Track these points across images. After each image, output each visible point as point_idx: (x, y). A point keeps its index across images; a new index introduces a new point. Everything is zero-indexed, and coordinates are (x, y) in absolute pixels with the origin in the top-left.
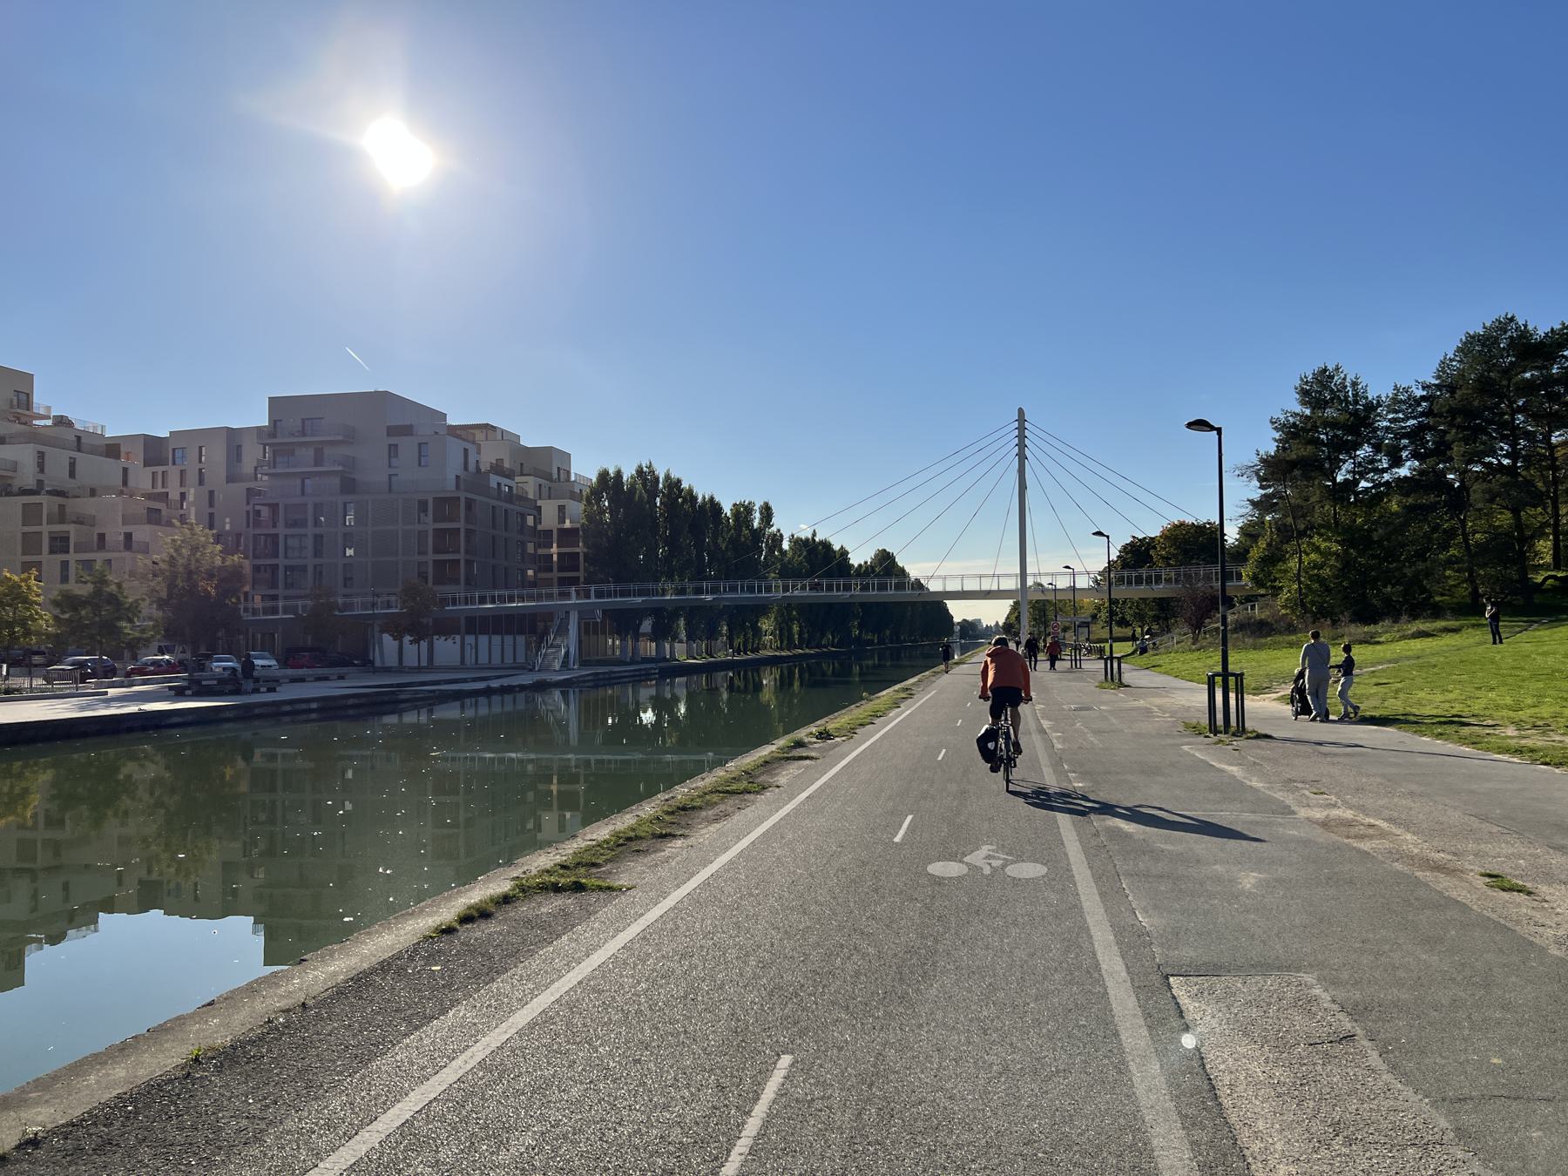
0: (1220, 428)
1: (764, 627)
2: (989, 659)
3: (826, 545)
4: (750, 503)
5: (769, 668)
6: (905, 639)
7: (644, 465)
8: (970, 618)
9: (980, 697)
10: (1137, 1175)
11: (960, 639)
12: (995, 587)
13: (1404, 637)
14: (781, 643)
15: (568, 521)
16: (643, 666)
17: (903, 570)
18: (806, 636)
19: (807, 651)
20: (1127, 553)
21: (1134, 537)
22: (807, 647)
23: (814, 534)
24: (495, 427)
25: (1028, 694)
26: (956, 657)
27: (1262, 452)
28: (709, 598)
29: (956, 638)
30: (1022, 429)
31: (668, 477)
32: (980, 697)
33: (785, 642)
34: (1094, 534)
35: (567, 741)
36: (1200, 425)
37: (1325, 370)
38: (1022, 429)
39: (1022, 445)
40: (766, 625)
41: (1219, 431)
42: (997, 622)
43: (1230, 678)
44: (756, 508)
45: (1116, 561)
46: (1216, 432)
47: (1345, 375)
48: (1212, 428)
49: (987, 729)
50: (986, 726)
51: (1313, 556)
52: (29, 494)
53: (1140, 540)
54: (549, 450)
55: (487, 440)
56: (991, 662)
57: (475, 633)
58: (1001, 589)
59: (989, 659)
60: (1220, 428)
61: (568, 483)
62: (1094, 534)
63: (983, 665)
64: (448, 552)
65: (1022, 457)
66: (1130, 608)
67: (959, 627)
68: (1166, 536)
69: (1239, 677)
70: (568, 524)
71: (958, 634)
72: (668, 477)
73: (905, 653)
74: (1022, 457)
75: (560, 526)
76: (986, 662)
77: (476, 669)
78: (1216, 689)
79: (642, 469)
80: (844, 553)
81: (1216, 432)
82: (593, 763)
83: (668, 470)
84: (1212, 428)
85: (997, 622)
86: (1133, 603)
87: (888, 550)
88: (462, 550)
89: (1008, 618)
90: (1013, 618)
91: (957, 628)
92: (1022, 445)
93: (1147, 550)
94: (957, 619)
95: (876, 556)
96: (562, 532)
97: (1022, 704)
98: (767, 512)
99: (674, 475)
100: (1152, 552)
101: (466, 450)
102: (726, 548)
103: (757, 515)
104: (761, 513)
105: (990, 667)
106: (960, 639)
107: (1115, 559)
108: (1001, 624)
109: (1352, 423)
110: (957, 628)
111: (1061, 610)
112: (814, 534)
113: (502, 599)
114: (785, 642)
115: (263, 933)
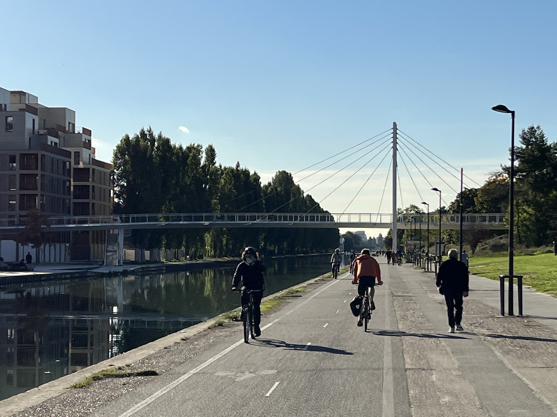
3: (246, 173)
4: (198, 146)
5: (173, 274)
7: (145, 130)
12: (378, 221)
13: (543, 253)
14: (215, 252)
15: (81, 163)
16: (144, 266)
17: (298, 188)
18: (231, 247)
19: (232, 258)
22: (230, 256)
23: (238, 166)
24: (25, 93)
27: (503, 165)
28: (207, 223)
30: (395, 133)
31: (160, 137)
33: (218, 251)
37: (533, 128)
38: (395, 133)
39: (395, 143)
40: (208, 238)
41: (513, 113)
43: (514, 278)
44: (203, 149)
45: (455, 203)
46: (511, 114)
47: (542, 131)
48: (509, 111)
51: (525, 214)
52: (92, 206)
53: (469, 190)
54: (63, 110)
55: (20, 103)
57: (60, 242)
58: (382, 222)
61: (73, 134)
64: (28, 189)
65: (395, 149)
67: (343, 239)
69: (520, 278)
70: (81, 165)
72: (160, 137)
74: (395, 149)
75: (76, 166)
77: (60, 264)
78: (514, 285)
79: (144, 132)
80: (257, 178)
81: (511, 114)
83: (161, 133)
84: (509, 111)
87: (287, 171)
88: (39, 187)
92: (395, 143)
96: (77, 170)
98: (211, 153)
99: (165, 135)
100: (475, 199)
101: (34, 120)
102: (191, 182)
103: (204, 155)
104: (207, 154)
109: (540, 156)
112: (238, 166)
113: (81, 222)
114: (218, 251)
115: (77, 367)
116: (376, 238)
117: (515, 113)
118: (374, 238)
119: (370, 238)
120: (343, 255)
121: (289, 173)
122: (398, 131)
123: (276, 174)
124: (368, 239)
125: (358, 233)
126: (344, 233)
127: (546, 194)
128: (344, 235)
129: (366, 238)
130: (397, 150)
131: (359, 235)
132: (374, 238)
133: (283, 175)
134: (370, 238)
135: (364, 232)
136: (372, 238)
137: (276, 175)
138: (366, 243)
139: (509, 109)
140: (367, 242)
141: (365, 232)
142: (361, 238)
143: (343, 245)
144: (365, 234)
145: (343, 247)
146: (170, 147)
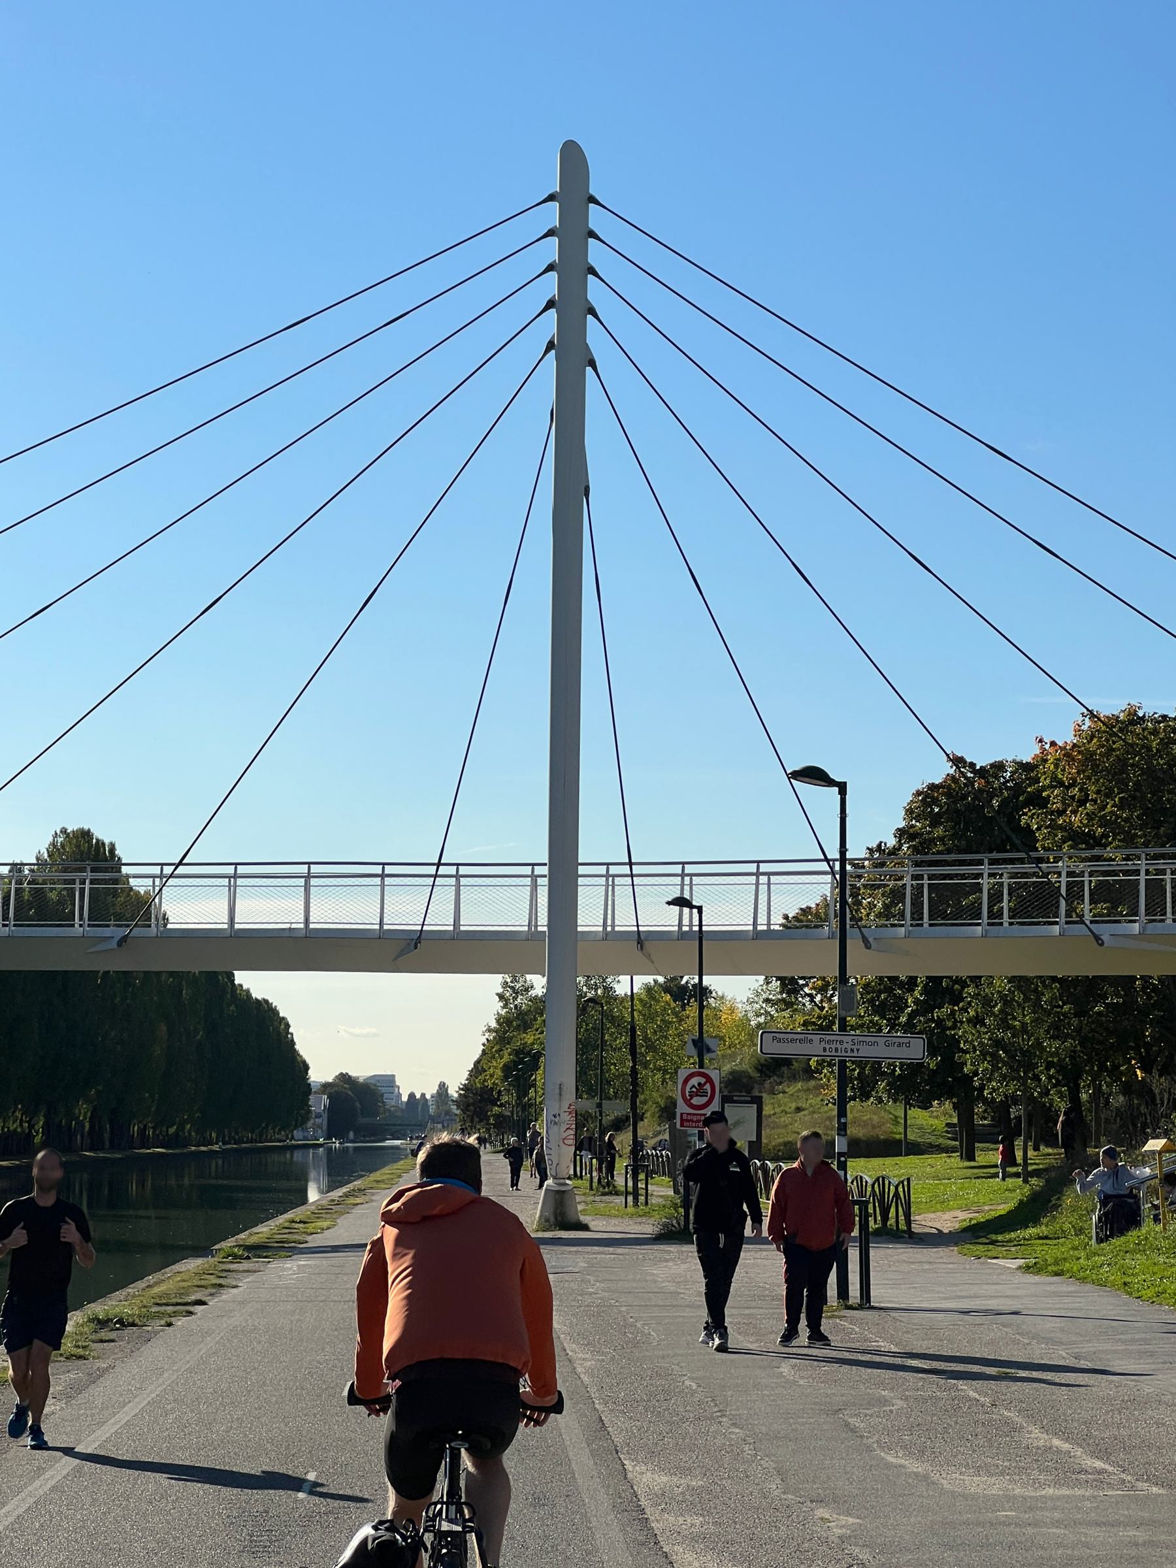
0: (845, 783)
1: (1121, 1098)
2: (391, 1233)
6: (142, 1132)
8: (361, 1071)
9: (353, 1399)
10: (611, 1567)
11: (329, 1137)
20: (935, 821)
21: (958, 761)
25: (545, 1381)
26: (313, 1195)
29: (314, 1131)
32: (353, 1399)
34: (669, 903)
35: (210, 1173)
36: (814, 775)
41: (842, 788)
42: (443, 1087)
45: (894, 851)
46: (836, 789)
48: (830, 782)
49: (364, 1542)
50: (367, 1531)
53: (982, 772)
56: (398, 1242)
59: (391, 1233)
60: (845, 783)
62: (669, 903)
63: (366, 1257)
66: (977, 1021)
68: (1089, 756)
71: (323, 1121)
73: (142, 1183)
76: (378, 1245)
81: (836, 789)
82: (351, 1150)
84: (830, 782)
85: (443, 1087)
86: (987, 1002)
89: (478, 1069)
90: (495, 1075)
91: (319, 1104)
93: (1011, 808)
94: (320, 1073)
95: (54, 850)
97: (523, 1431)
100: (1030, 819)
105: (392, 1269)
106: (329, 1137)
107: (891, 842)
108: (453, 1092)
110: (319, 1104)
111: (651, 1047)
116: (428, 1097)
117: (704, 909)
118: (423, 1095)
119: (412, 1096)
120: (1137, 924)
121: (107, 842)
122: (596, 218)
123: (51, 839)
124: (405, 1098)
125: (373, 1081)
126: (330, 1080)
127: (958, 1006)
128: (326, 1086)
129: (400, 1095)
130: (592, 364)
131: (375, 1085)
132: (423, 1095)
133: (78, 846)
134: (412, 1096)
135: (394, 1076)
136: (418, 1096)
137: (54, 844)
138: (399, 1114)
139: (833, 776)
140: (402, 1110)
141: (397, 1079)
142: (382, 1095)
143: (325, 1116)
144: (397, 1084)
145: (325, 1123)
146: (447, 1094)
